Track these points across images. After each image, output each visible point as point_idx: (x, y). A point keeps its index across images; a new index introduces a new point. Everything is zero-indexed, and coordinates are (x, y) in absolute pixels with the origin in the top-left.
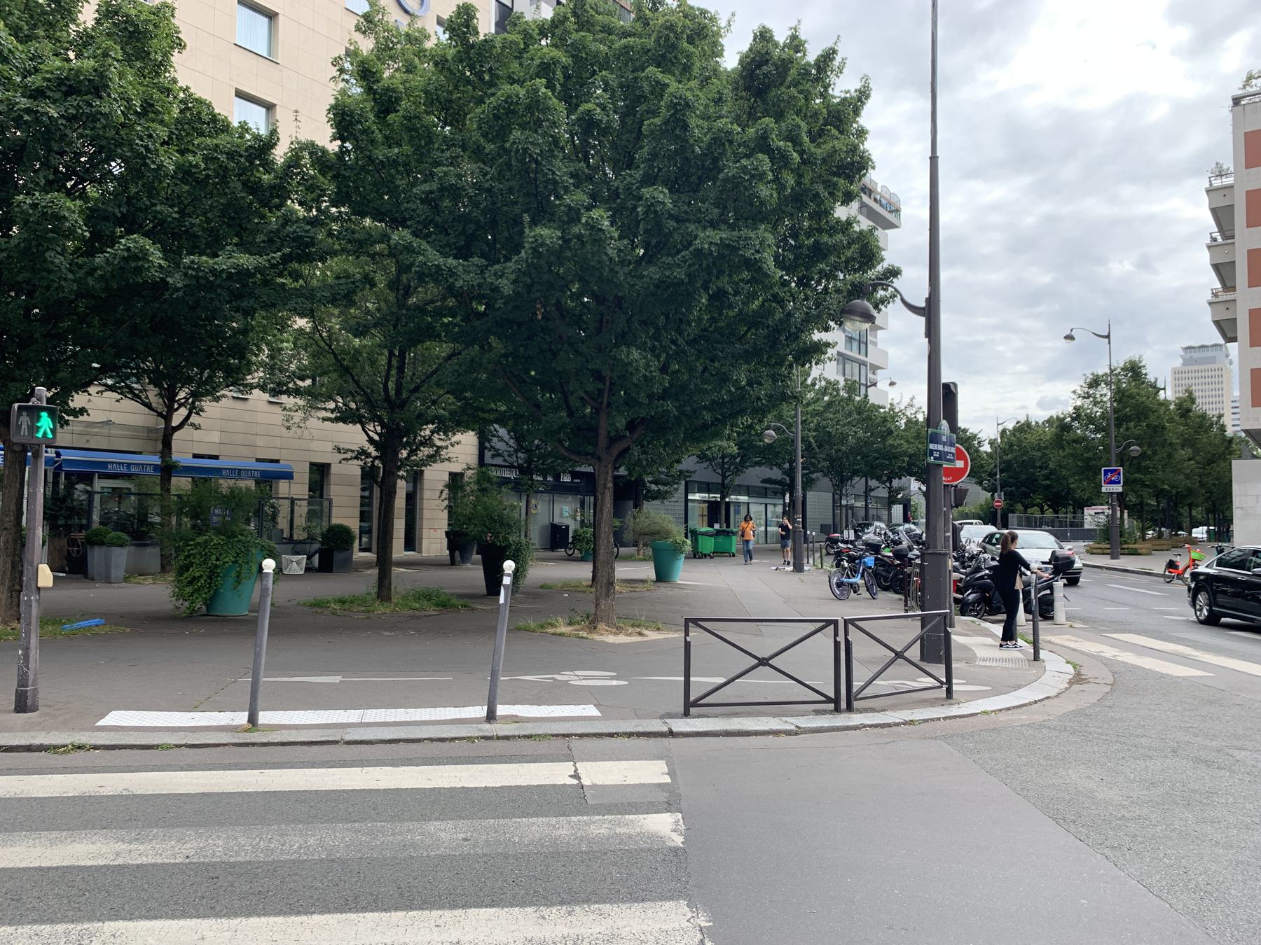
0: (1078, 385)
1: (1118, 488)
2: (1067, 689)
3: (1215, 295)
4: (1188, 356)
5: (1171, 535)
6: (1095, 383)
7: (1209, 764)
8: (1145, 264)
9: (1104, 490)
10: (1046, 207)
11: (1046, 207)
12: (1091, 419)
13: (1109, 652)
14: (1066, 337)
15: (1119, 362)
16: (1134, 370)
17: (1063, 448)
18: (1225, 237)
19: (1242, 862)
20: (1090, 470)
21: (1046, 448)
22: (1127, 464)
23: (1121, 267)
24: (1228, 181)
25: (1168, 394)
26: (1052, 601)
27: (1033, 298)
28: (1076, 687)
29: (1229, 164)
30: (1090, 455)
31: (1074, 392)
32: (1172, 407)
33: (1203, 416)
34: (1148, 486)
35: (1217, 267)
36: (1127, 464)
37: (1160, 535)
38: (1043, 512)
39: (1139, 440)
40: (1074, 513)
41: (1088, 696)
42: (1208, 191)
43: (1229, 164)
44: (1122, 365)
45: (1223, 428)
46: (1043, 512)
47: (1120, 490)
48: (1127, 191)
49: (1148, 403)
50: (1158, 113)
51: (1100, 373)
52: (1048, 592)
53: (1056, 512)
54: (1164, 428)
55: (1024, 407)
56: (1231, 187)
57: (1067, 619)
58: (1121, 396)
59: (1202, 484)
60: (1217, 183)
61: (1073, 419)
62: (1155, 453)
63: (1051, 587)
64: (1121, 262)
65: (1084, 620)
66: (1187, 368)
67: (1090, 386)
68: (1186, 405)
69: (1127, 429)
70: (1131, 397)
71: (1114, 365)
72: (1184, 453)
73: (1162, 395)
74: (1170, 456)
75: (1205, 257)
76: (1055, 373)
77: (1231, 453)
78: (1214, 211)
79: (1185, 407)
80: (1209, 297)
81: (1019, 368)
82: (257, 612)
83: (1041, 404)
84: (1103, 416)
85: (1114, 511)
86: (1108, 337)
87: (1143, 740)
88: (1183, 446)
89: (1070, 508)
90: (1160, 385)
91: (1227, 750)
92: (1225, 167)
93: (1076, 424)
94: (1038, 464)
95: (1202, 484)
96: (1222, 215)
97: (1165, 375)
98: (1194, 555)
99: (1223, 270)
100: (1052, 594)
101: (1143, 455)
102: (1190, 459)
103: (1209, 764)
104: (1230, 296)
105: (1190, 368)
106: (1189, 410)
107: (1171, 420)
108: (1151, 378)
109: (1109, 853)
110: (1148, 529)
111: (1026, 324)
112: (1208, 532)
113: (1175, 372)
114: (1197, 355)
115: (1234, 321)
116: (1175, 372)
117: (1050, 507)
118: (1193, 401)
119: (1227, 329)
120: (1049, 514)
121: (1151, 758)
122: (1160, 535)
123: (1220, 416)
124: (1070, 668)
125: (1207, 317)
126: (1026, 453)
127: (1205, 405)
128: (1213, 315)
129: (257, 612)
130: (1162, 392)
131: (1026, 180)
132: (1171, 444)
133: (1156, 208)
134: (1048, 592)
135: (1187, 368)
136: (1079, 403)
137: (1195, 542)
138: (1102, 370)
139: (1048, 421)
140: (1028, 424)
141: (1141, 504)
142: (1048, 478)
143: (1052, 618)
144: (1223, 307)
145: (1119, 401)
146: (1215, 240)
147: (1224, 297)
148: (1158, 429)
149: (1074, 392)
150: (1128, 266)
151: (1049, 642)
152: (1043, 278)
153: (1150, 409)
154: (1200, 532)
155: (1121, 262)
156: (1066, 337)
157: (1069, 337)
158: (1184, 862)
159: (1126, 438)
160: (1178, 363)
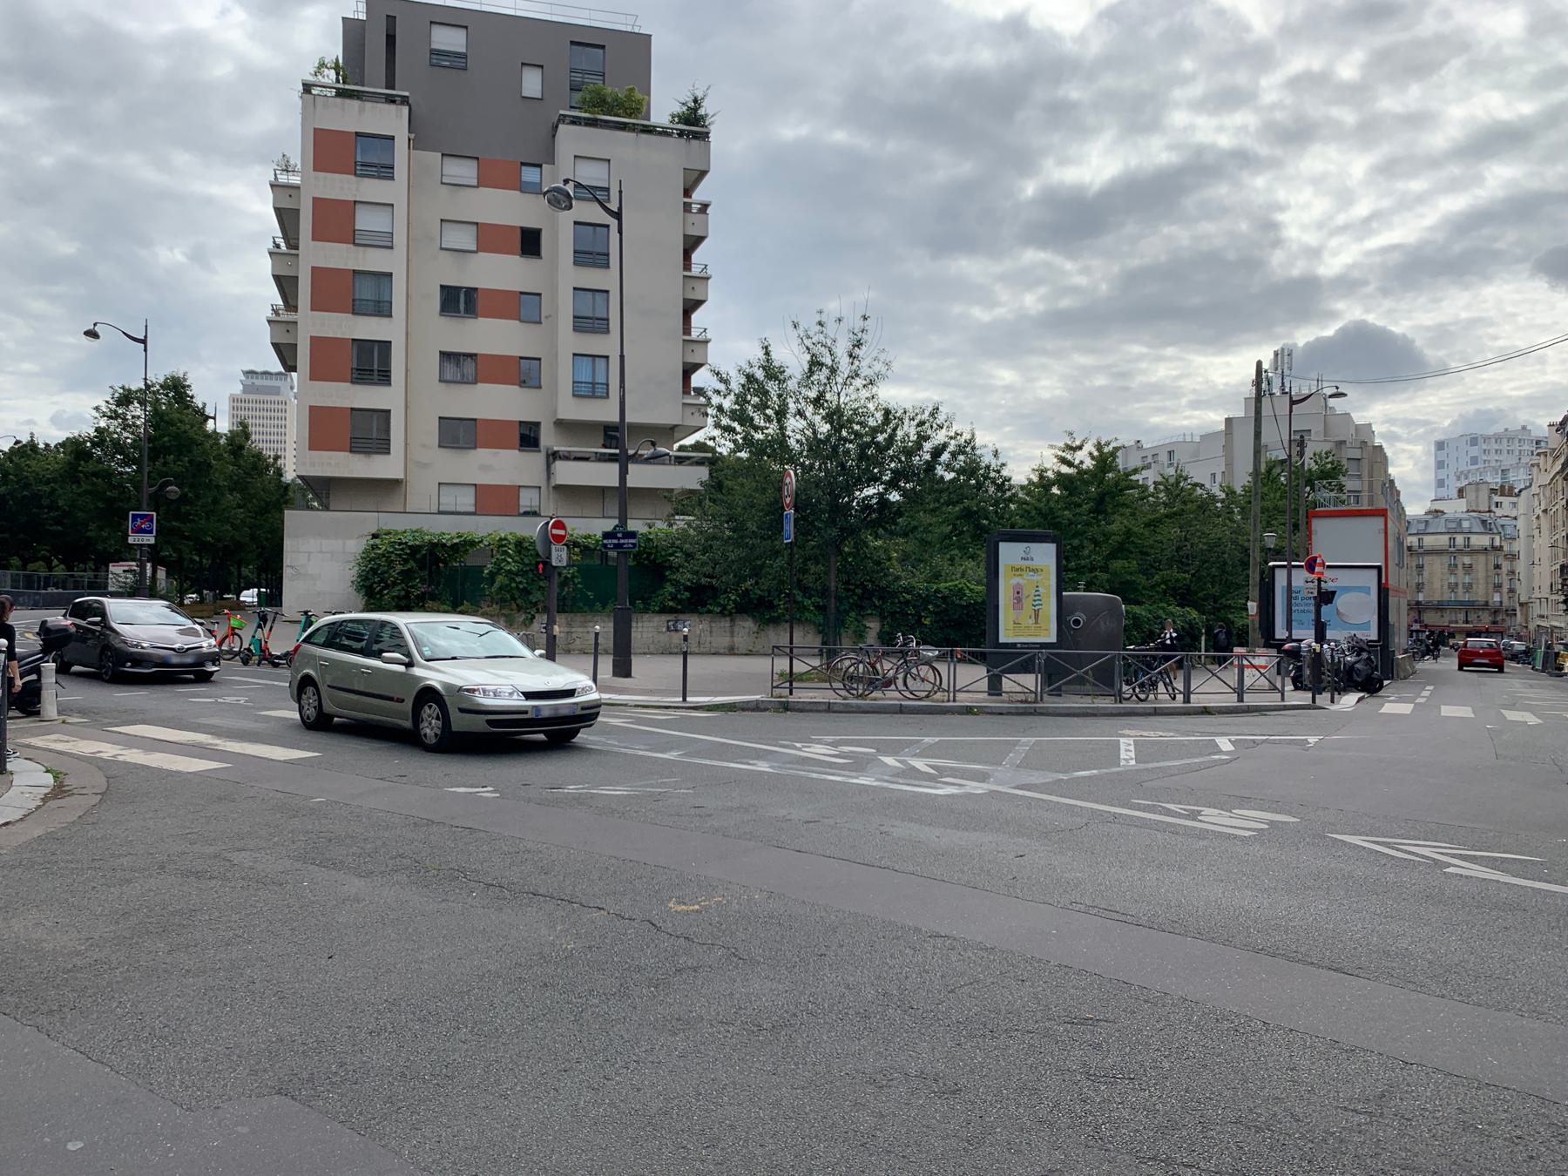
0: (103, 399)
1: (150, 539)
2: (38, 808)
3: (276, 312)
4: (249, 382)
5: (215, 597)
6: (125, 399)
7: (198, 875)
8: (199, 256)
9: (131, 540)
10: (71, 149)
11: (71, 149)
12: (118, 446)
13: (108, 751)
14: (87, 333)
15: (158, 376)
16: (177, 387)
17: (77, 481)
18: (289, 246)
19: (212, 988)
20: (114, 515)
21: (54, 480)
22: (162, 510)
23: (170, 255)
24: (295, 180)
25: (222, 425)
26: (39, 689)
27: (50, 272)
28: (53, 804)
29: (296, 160)
30: (115, 493)
31: (97, 409)
32: (223, 441)
33: (259, 456)
34: (187, 538)
35: (278, 279)
36: (162, 510)
37: (202, 600)
38: (50, 569)
39: (179, 480)
40: (96, 570)
41: (70, 810)
42: (272, 186)
43: (296, 160)
44: (161, 380)
45: (279, 473)
46: (50, 569)
47: (152, 541)
48: (181, 158)
49: (191, 433)
50: (222, 70)
51: (134, 388)
52: (34, 677)
53: (70, 569)
54: (209, 466)
55: (31, 422)
56: (297, 188)
57: (59, 713)
58: (158, 419)
59: (253, 538)
60: (283, 178)
61: (94, 445)
62: (198, 497)
63: (37, 670)
64: (171, 249)
65: (82, 712)
66: (247, 397)
67: (119, 403)
68: (238, 441)
69: (165, 464)
70: (171, 423)
71: (151, 378)
72: (232, 499)
73: (210, 425)
74: (215, 501)
75: (266, 266)
76: (75, 381)
77: (286, 502)
78: (278, 211)
79: (239, 440)
80: (269, 313)
81: (27, 366)
82: (467, 311)
83: (56, 420)
84: (134, 445)
85: (142, 567)
86: (144, 341)
87: (124, 861)
88: (231, 490)
89: (91, 565)
90: (209, 411)
91: (226, 854)
92: (292, 162)
93: (98, 452)
94: (45, 502)
95: (253, 538)
96: (287, 218)
97: (218, 401)
98: (234, 623)
99: (286, 284)
100: (39, 680)
101: (183, 499)
102: (239, 506)
103: (198, 875)
104: (290, 317)
105: (251, 397)
106: (241, 447)
107: (219, 457)
108: (198, 402)
109: (43, 1021)
110: (187, 591)
111: (38, 306)
112: (259, 594)
113: (234, 399)
114: (259, 382)
115: (293, 347)
116: (234, 399)
117: (61, 562)
118: (247, 436)
119: (286, 353)
120: (60, 571)
121: (129, 881)
122: (202, 600)
123: (277, 458)
124: (49, 779)
125: (265, 335)
126: (27, 486)
127: (260, 441)
128: (272, 337)
129: (467, 311)
130: (211, 422)
131: (40, 102)
132: (217, 487)
133: (215, 190)
134: (34, 677)
135: (247, 397)
136: (103, 424)
137: (240, 607)
138: (137, 385)
139: (63, 445)
140: (32, 446)
141: (181, 559)
142: (58, 523)
143: (38, 713)
144: (283, 328)
145: (156, 427)
146: (278, 246)
147: (285, 317)
148: (202, 468)
149: (97, 409)
150: (179, 256)
151: (29, 746)
152: (67, 249)
153: (193, 441)
154: (249, 596)
155: (171, 249)
156: (87, 333)
157: (92, 334)
158: (142, 1007)
159: (162, 475)
160: (237, 389)
